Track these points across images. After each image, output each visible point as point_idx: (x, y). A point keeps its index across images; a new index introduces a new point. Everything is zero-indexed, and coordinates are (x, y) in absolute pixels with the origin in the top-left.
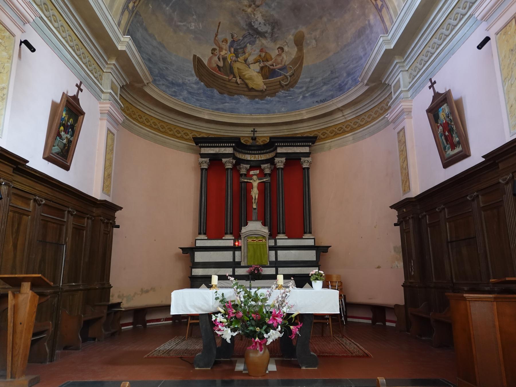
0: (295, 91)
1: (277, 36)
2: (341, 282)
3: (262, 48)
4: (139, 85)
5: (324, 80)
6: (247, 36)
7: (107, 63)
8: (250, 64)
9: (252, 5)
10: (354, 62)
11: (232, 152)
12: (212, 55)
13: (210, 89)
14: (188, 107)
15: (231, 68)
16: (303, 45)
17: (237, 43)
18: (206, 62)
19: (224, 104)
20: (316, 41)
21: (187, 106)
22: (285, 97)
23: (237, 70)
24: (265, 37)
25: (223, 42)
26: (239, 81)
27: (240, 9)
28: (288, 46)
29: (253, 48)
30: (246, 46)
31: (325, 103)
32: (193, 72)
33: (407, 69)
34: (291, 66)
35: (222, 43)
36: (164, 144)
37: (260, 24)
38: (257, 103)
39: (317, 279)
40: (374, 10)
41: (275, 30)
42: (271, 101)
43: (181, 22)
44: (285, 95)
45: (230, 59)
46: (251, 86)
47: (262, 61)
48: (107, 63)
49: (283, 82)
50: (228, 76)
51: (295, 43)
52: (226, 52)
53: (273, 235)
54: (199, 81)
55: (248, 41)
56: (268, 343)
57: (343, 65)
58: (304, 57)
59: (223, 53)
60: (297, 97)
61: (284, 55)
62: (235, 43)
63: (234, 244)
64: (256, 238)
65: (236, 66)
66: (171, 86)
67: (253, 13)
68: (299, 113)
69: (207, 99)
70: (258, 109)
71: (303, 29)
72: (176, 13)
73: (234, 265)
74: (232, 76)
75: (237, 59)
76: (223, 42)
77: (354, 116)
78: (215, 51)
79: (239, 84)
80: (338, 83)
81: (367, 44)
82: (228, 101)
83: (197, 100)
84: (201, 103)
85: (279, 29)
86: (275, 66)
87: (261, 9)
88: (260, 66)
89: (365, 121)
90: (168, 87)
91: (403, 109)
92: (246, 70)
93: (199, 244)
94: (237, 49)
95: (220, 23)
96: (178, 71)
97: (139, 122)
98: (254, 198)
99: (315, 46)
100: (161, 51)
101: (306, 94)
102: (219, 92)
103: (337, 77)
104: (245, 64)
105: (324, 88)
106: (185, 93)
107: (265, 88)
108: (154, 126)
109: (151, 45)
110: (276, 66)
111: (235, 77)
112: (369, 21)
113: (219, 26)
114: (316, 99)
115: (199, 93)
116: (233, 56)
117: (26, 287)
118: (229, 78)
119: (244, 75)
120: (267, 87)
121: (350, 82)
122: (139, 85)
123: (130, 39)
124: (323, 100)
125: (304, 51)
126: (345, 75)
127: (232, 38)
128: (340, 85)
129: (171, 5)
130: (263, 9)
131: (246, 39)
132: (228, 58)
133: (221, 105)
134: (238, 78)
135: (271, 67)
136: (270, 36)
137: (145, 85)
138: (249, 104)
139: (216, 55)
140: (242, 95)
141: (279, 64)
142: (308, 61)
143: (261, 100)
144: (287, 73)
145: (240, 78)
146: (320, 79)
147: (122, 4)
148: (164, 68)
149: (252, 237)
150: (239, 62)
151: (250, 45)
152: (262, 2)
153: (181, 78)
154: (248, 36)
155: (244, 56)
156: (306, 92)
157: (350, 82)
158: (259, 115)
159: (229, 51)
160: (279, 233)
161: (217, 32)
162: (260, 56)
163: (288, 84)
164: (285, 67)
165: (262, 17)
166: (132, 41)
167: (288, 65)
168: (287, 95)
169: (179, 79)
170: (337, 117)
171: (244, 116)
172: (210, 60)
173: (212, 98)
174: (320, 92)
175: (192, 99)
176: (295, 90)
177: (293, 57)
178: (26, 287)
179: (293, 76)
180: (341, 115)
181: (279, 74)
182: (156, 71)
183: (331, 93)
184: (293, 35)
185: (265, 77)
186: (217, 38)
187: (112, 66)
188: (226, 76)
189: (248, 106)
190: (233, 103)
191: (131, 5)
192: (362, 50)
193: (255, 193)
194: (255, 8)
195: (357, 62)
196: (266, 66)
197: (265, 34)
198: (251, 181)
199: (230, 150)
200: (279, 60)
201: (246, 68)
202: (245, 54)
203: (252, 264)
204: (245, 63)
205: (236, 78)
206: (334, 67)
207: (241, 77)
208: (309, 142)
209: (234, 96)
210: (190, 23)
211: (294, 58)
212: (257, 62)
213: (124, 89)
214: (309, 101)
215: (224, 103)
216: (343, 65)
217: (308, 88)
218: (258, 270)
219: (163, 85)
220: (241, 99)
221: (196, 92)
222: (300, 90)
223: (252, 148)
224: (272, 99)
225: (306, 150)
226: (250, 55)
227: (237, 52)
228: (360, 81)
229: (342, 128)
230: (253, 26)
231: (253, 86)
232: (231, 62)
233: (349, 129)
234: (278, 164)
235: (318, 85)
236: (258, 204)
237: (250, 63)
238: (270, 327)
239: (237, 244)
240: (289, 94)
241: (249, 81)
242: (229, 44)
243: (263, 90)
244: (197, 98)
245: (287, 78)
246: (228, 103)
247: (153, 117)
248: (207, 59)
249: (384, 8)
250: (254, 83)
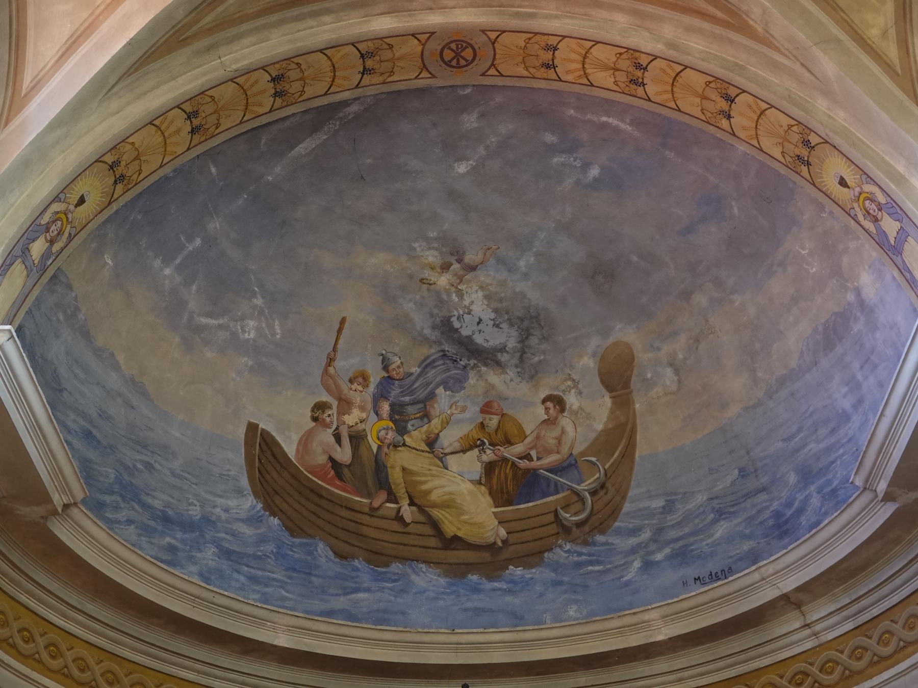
0: (613, 544)
1: (540, 361)
3: (487, 400)
4: (33, 512)
5: (716, 501)
6: (434, 361)
8: (446, 454)
9: (451, 265)
10: (822, 432)
12: (314, 424)
13: (304, 541)
14: (215, 600)
15: (380, 468)
16: (632, 386)
17: (401, 386)
18: (290, 449)
19: (354, 596)
20: (677, 371)
21: (209, 596)
22: (579, 565)
23: (401, 474)
24: (498, 364)
25: (351, 381)
26: (407, 512)
27: (411, 277)
28: (580, 393)
29: (456, 402)
30: (432, 396)
31: (731, 579)
32: (244, 482)
34: (594, 459)
35: (349, 385)
37: (478, 323)
38: (476, 590)
40: (872, 252)
41: (533, 341)
42: (527, 584)
43: (209, 315)
44: (576, 559)
45: (378, 439)
46: (450, 529)
47: (491, 444)
49: (568, 515)
50: (369, 496)
51: (602, 381)
52: (364, 415)
54: (262, 512)
55: (438, 379)
57: (780, 444)
58: (639, 428)
59: (351, 418)
60: (623, 565)
61: (565, 422)
62: (393, 384)
65: (399, 460)
66: (160, 528)
67: (457, 288)
68: (634, 619)
69: (290, 577)
70: (478, 611)
72: (194, 287)
74: (383, 496)
75: (400, 438)
76: (351, 381)
78: (323, 412)
79: (406, 524)
80: (772, 509)
81: (862, 368)
82: (366, 585)
83: (253, 579)
84: (266, 589)
85: (544, 339)
86: (535, 459)
87: (482, 276)
88: (482, 462)
89: (894, 640)
90: (146, 530)
92: (432, 475)
94: (403, 405)
95: (343, 321)
96: (190, 477)
97: (20, 653)
99: (674, 388)
100: (132, 407)
101: (653, 552)
102: (335, 553)
103: (764, 489)
104: (431, 455)
105: (721, 530)
106: (209, 555)
107: (501, 535)
108: (76, 673)
109: (98, 384)
110: (539, 459)
112: (858, 292)
113: (340, 331)
114: (691, 572)
115: (260, 554)
116: (387, 429)
118: (371, 503)
119: (429, 492)
120: (507, 533)
121: (815, 501)
122: (33, 512)
123: (12, 337)
124: (719, 574)
125: (637, 406)
126: (792, 478)
127: (386, 368)
128: (777, 514)
129: (178, 261)
130: (490, 276)
131: (431, 373)
132: (369, 434)
133: (342, 598)
134: (405, 503)
135: (524, 464)
136: (515, 361)
137: (55, 513)
138: (443, 593)
139: (327, 426)
140: (417, 561)
141: (549, 452)
143: (491, 579)
144: (582, 482)
145: (412, 503)
146: (701, 498)
147: (7, 241)
148: (139, 466)
150: (409, 447)
151: (448, 393)
152: (485, 254)
153: (198, 500)
154: (440, 362)
155: (426, 427)
156: (653, 547)
157: (815, 501)
158: (482, 630)
159: (372, 412)
162: (482, 425)
164: (573, 462)
165: (486, 302)
166: (15, 342)
167: (582, 454)
168: (584, 557)
169: (192, 504)
170: (783, 631)
171: (427, 638)
172: (305, 441)
173: (310, 574)
174: (705, 543)
175: (235, 575)
176: (614, 542)
177: (599, 427)
179: (602, 493)
180: (797, 625)
181: (552, 486)
182: (108, 473)
183: (746, 546)
184: (594, 356)
185: (501, 497)
186: (331, 370)
188: (362, 497)
189: (441, 603)
190: (386, 591)
191: (38, 248)
192: (844, 390)
194: (462, 273)
195: (833, 431)
196: (505, 460)
197: (499, 355)
200: (550, 436)
201: (434, 468)
202: (430, 421)
204: (429, 452)
205: (396, 502)
206: (748, 453)
207: (416, 501)
209: (387, 565)
210: (243, 318)
211: (602, 431)
212: (471, 448)
214: (669, 576)
215: (352, 593)
216: (780, 444)
217: (660, 530)
219: (130, 522)
220: (413, 577)
221: (250, 551)
222: (633, 541)
224: (530, 576)
226: (446, 423)
227: (401, 413)
228: (857, 488)
229: (808, 675)
230: (457, 329)
231: (459, 529)
232: (379, 447)
233: (835, 676)
235: (696, 521)
237: (447, 451)
240: (590, 555)
241: (444, 513)
242: (372, 388)
243: (495, 543)
244: (252, 571)
245: (582, 500)
246: (368, 590)
247: (78, 638)
248: (295, 437)
249: (910, 239)
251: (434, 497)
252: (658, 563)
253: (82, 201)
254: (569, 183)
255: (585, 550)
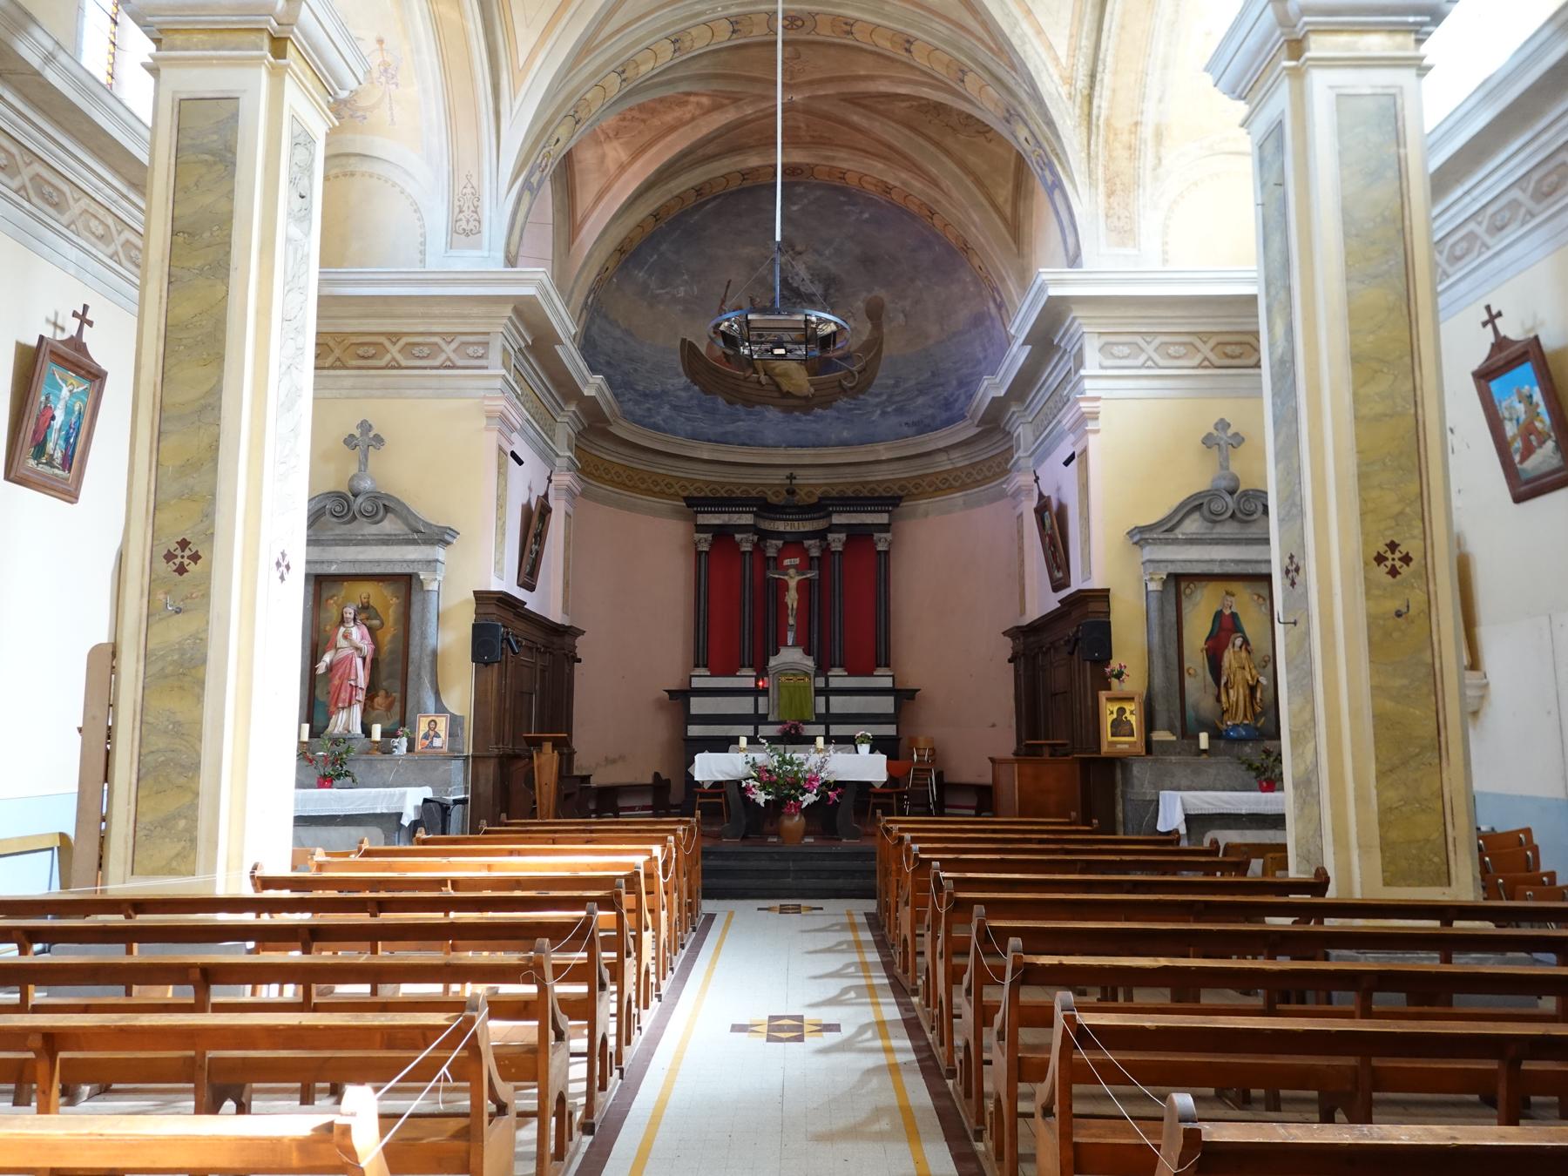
2: (933, 750)
7: (563, 410)
11: (751, 522)
18: (703, 350)
20: (906, 316)
22: (850, 410)
26: (763, 379)
32: (681, 369)
33: (1030, 420)
36: (631, 508)
38: (798, 420)
39: (863, 742)
41: (832, 291)
43: (662, 288)
46: (785, 388)
48: (563, 410)
53: (822, 668)
56: (804, 806)
63: (757, 685)
64: (794, 675)
71: (881, 293)
73: (757, 719)
74: (751, 371)
77: (967, 463)
91: (1019, 487)
93: (697, 683)
95: (729, 282)
98: (790, 607)
103: (942, 385)
105: (920, 400)
106: (666, 409)
111: (756, 371)
113: (728, 286)
117: (548, 746)
126: (954, 383)
142: (893, 347)
143: (805, 414)
146: (912, 382)
149: (786, 675)
160: (834, 666)
161: (725, 296)
163: (854, 387)
167: (855, 352)
172: (710, 347)
177: (864, 338)
178: (548, 746)
185: (812, 371)
187: (571, 414)
193: (792, 598)
198: (786, 578)
199: (747, 519)
203: (786, 718)
208: (888, 505)
209: (753, 407)
213: (583, 437)
217: (890, 396)
218: (797, 729)
219: (630, 400)
220: (767, 413)
222: (877, 400)
223: (788, 510)
225: (883, 518)
234: (833, 545)
236: (798, 617)
238: (805, 791)
239: (761, 683)
245: (854, 376)
246: (743, 420)
250: (793, 382)
251: (777, 371)
252: (889, 413)
253: (558, 140)
254: (853, 218)
255: (853, 402)
